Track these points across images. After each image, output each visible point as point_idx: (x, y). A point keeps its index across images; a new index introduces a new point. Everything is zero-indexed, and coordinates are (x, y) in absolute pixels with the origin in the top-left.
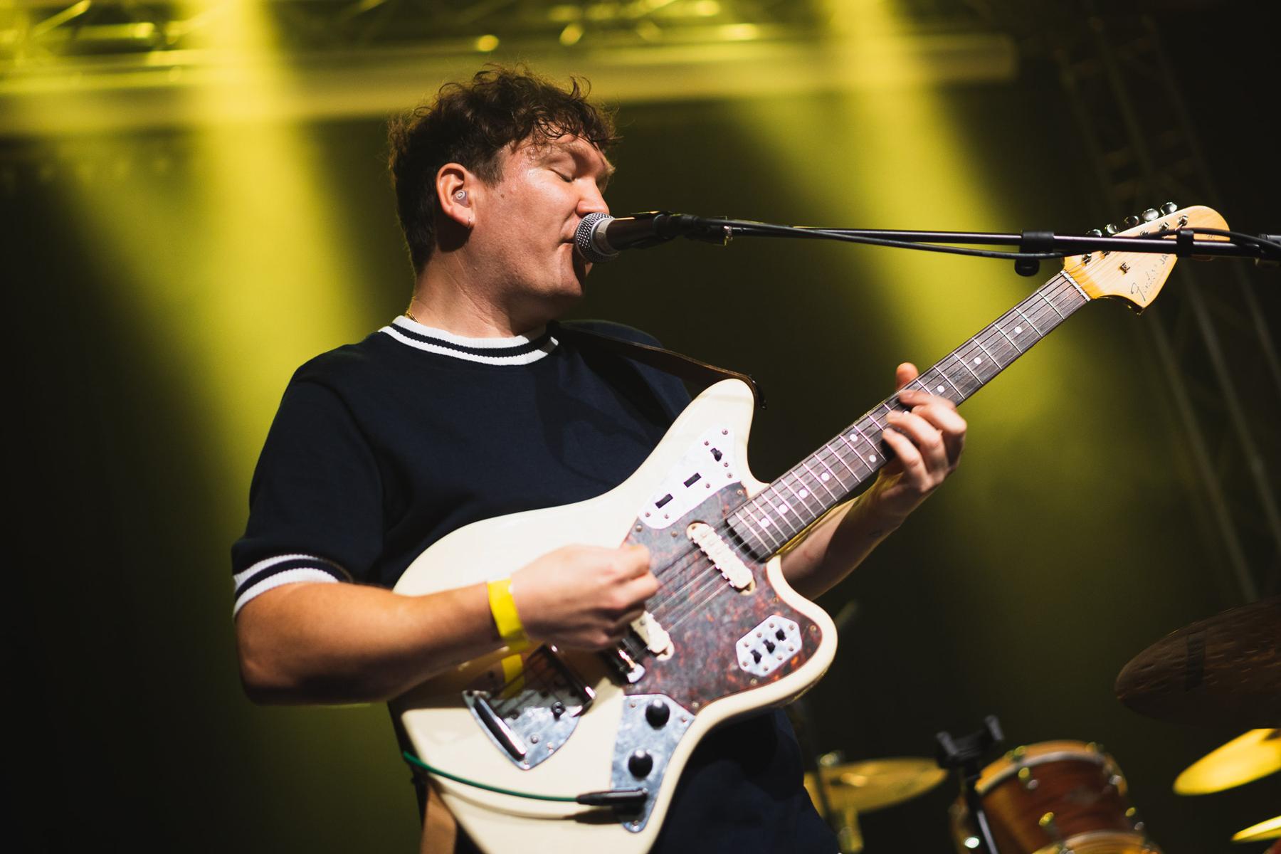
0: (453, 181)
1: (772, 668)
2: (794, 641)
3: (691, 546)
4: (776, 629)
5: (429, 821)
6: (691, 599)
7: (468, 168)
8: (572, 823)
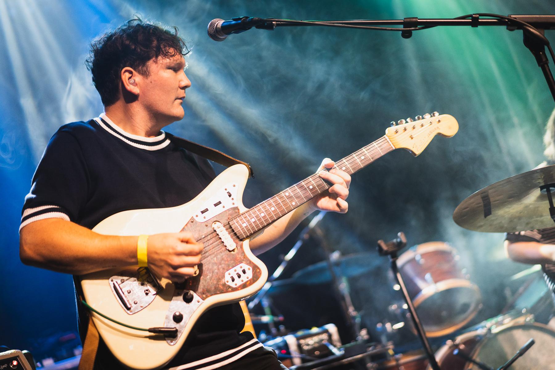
0: (127, 75)
1: (238, 285)
2: (250, 274)
3: (213, 231)
4: (242, 269)
5: (89, 333)
6: (210, 252)
7: (135, 69)
8: (147, 339)
